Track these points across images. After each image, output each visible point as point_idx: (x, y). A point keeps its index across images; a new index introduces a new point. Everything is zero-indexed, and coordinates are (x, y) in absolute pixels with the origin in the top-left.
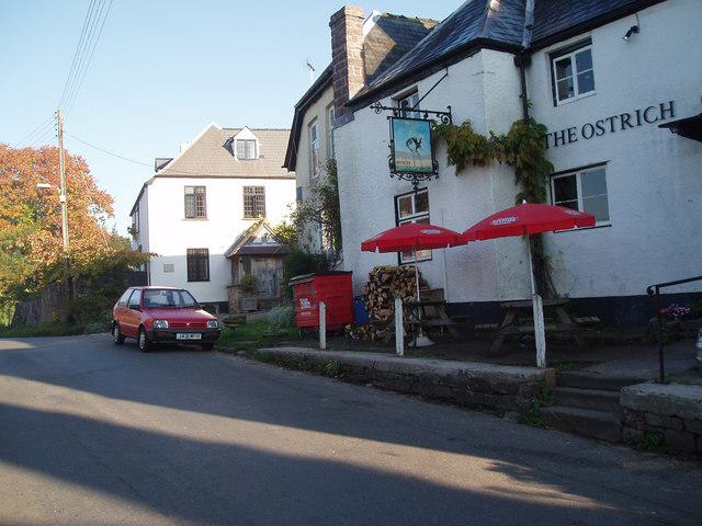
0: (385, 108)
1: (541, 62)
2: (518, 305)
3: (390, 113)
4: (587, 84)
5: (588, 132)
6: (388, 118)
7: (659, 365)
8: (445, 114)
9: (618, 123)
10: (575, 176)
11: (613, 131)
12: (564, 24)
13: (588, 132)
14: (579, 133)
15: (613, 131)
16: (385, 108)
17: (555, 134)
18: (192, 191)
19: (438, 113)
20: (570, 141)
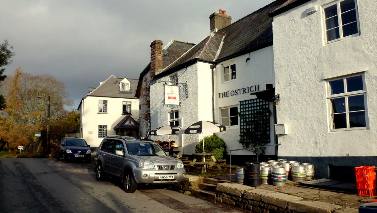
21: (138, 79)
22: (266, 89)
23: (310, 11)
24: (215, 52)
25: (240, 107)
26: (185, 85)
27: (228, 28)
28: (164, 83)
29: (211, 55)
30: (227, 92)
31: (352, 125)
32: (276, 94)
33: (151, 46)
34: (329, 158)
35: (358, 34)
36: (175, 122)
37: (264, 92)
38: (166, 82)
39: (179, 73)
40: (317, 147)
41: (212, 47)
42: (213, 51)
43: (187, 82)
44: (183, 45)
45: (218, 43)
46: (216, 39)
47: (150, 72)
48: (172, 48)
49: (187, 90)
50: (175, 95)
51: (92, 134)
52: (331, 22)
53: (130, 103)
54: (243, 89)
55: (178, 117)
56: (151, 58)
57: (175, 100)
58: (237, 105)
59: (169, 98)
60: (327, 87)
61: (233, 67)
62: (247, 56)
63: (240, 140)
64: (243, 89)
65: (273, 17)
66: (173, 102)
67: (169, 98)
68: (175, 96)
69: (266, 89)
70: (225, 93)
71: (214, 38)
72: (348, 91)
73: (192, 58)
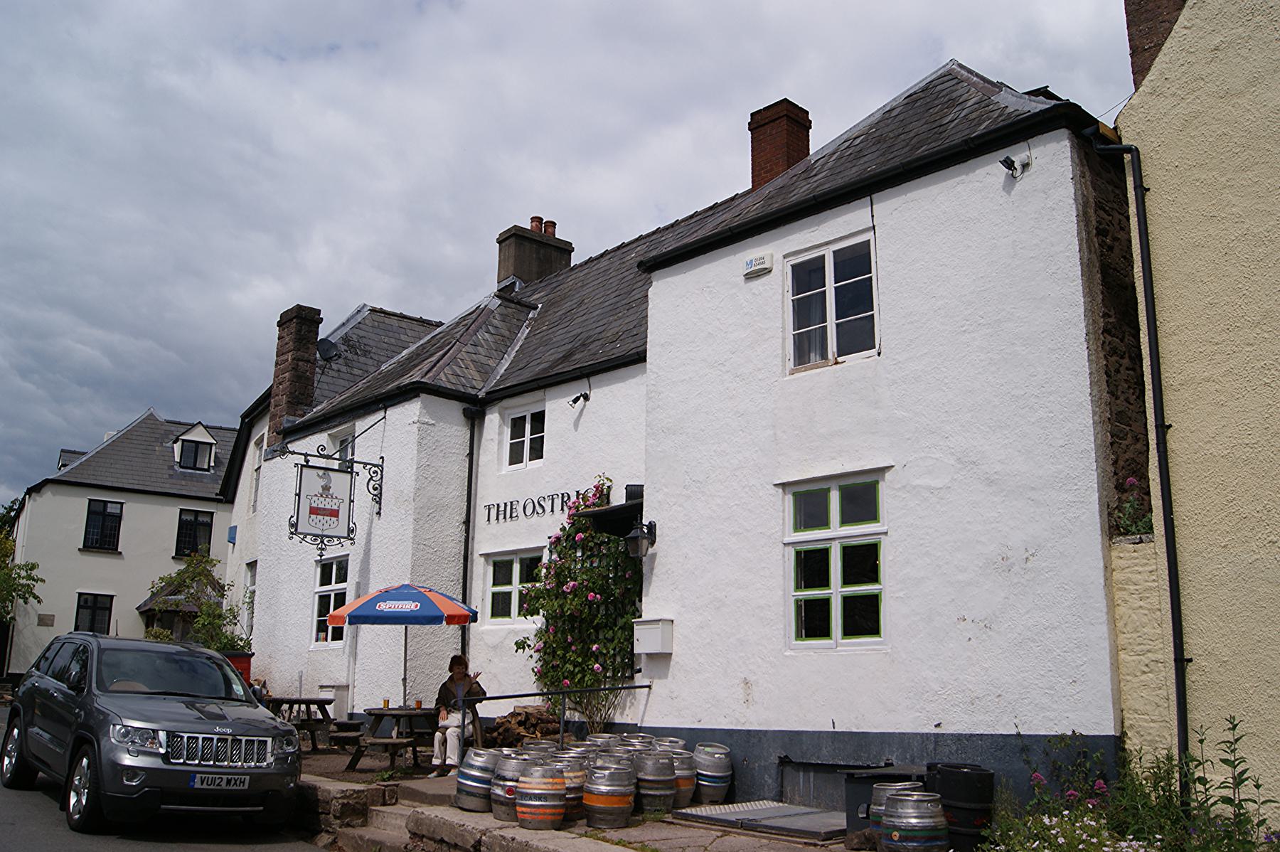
0: (293, 453)
1: (493, 420)
2: (376, 712)
3: (301, 460)
4: (537, 452)
5: (529, 510)
6: (296, 465)
7: (637, 690)
8: (375, 466)
9: (558, 502)
10: (330, 595)
11: (552, 511)
12: (451, 352)
13: (529, 510)
14: (520, 509)
15: (552, 511)
16: (293, 453)
17: (498, 505)
18: (190, 518)
19: (366, 464)
20: (511, 517)
21: (234, 430)
22: (624, 502)
23: (753, 268)
24: (491, 362)
25: (551, 558)
26: (373, 469)
27: (842, 169)
28: (301, 460)
29: (473, 373)
30: (511, 503)
31: (849, 631)
32: (645, 522)
33: (279, 324)
34: (791, 731)
35: (874, 352)
36: (336, 595)
37: (620, 508)
38: (306, 455)
39: (360, 425)
40: (750, 698)
41: (483, 347)
42: (484, 360)
43: (382, 458)
44: (403, 324)
45: (507, 333)
46: (504, 318)
47: (267, 419)
48: (362, 333)
49: (381, 486)
50: (335, 501)
51: (52, 626)
52: (807, 311)
53: (206, 519)
54: (563, 494)
55: (345, 581)
56: (277, 364)
57: (334, 519)
58: (541, 549)
59: (314, 511)
60: (786, 506)
61: (539, 419)
62: (579, 388)
63: (240, 631)
64: (563, 494)
65: (653, 274)
66: (327, 526)
67: (314, 511)
68: (335, 507)
69: (624, 502)
70: (505, 504)
71: (497, 316)
72: (845, 520)
73: (406, 380)
